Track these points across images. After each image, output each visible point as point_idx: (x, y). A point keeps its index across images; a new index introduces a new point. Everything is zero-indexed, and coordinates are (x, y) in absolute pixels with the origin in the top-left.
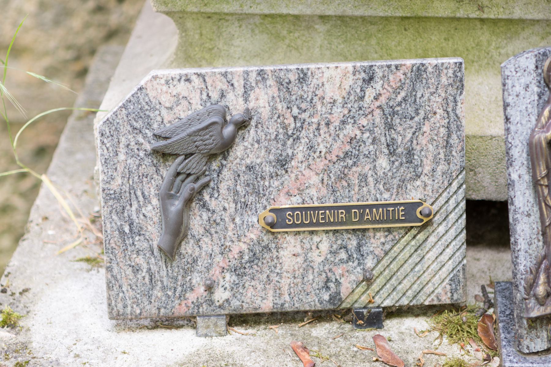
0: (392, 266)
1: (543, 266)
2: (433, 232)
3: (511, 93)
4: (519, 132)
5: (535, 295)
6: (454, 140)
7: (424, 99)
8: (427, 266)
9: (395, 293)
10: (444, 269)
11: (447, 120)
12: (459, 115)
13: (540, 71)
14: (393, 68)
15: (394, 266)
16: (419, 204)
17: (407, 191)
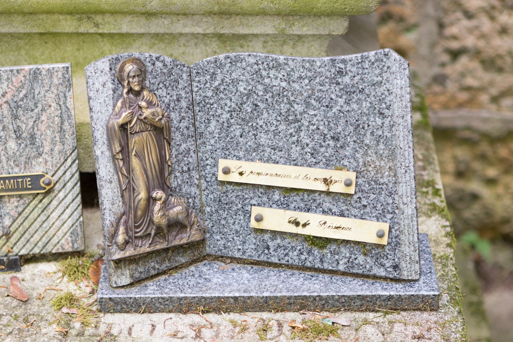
0: (24, 224)
1: (122, 221)
2: (55, 196)
3: (92, 89)
4: (100, 119)
5: (116, 243)
6: (66, 126)
7: (40, 96)
8: (52, 223)
9: (28, 244)
10: (65, 225)
11: (60, 111)
12: (69, 107)
13: (113, 72)
14: (15, 72)
15: (26, 224)
16: (42, 176)
17: (33, 166)
